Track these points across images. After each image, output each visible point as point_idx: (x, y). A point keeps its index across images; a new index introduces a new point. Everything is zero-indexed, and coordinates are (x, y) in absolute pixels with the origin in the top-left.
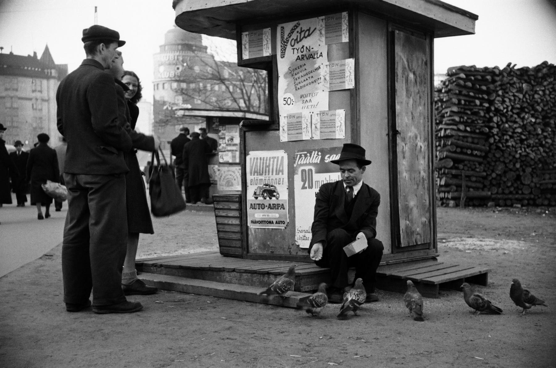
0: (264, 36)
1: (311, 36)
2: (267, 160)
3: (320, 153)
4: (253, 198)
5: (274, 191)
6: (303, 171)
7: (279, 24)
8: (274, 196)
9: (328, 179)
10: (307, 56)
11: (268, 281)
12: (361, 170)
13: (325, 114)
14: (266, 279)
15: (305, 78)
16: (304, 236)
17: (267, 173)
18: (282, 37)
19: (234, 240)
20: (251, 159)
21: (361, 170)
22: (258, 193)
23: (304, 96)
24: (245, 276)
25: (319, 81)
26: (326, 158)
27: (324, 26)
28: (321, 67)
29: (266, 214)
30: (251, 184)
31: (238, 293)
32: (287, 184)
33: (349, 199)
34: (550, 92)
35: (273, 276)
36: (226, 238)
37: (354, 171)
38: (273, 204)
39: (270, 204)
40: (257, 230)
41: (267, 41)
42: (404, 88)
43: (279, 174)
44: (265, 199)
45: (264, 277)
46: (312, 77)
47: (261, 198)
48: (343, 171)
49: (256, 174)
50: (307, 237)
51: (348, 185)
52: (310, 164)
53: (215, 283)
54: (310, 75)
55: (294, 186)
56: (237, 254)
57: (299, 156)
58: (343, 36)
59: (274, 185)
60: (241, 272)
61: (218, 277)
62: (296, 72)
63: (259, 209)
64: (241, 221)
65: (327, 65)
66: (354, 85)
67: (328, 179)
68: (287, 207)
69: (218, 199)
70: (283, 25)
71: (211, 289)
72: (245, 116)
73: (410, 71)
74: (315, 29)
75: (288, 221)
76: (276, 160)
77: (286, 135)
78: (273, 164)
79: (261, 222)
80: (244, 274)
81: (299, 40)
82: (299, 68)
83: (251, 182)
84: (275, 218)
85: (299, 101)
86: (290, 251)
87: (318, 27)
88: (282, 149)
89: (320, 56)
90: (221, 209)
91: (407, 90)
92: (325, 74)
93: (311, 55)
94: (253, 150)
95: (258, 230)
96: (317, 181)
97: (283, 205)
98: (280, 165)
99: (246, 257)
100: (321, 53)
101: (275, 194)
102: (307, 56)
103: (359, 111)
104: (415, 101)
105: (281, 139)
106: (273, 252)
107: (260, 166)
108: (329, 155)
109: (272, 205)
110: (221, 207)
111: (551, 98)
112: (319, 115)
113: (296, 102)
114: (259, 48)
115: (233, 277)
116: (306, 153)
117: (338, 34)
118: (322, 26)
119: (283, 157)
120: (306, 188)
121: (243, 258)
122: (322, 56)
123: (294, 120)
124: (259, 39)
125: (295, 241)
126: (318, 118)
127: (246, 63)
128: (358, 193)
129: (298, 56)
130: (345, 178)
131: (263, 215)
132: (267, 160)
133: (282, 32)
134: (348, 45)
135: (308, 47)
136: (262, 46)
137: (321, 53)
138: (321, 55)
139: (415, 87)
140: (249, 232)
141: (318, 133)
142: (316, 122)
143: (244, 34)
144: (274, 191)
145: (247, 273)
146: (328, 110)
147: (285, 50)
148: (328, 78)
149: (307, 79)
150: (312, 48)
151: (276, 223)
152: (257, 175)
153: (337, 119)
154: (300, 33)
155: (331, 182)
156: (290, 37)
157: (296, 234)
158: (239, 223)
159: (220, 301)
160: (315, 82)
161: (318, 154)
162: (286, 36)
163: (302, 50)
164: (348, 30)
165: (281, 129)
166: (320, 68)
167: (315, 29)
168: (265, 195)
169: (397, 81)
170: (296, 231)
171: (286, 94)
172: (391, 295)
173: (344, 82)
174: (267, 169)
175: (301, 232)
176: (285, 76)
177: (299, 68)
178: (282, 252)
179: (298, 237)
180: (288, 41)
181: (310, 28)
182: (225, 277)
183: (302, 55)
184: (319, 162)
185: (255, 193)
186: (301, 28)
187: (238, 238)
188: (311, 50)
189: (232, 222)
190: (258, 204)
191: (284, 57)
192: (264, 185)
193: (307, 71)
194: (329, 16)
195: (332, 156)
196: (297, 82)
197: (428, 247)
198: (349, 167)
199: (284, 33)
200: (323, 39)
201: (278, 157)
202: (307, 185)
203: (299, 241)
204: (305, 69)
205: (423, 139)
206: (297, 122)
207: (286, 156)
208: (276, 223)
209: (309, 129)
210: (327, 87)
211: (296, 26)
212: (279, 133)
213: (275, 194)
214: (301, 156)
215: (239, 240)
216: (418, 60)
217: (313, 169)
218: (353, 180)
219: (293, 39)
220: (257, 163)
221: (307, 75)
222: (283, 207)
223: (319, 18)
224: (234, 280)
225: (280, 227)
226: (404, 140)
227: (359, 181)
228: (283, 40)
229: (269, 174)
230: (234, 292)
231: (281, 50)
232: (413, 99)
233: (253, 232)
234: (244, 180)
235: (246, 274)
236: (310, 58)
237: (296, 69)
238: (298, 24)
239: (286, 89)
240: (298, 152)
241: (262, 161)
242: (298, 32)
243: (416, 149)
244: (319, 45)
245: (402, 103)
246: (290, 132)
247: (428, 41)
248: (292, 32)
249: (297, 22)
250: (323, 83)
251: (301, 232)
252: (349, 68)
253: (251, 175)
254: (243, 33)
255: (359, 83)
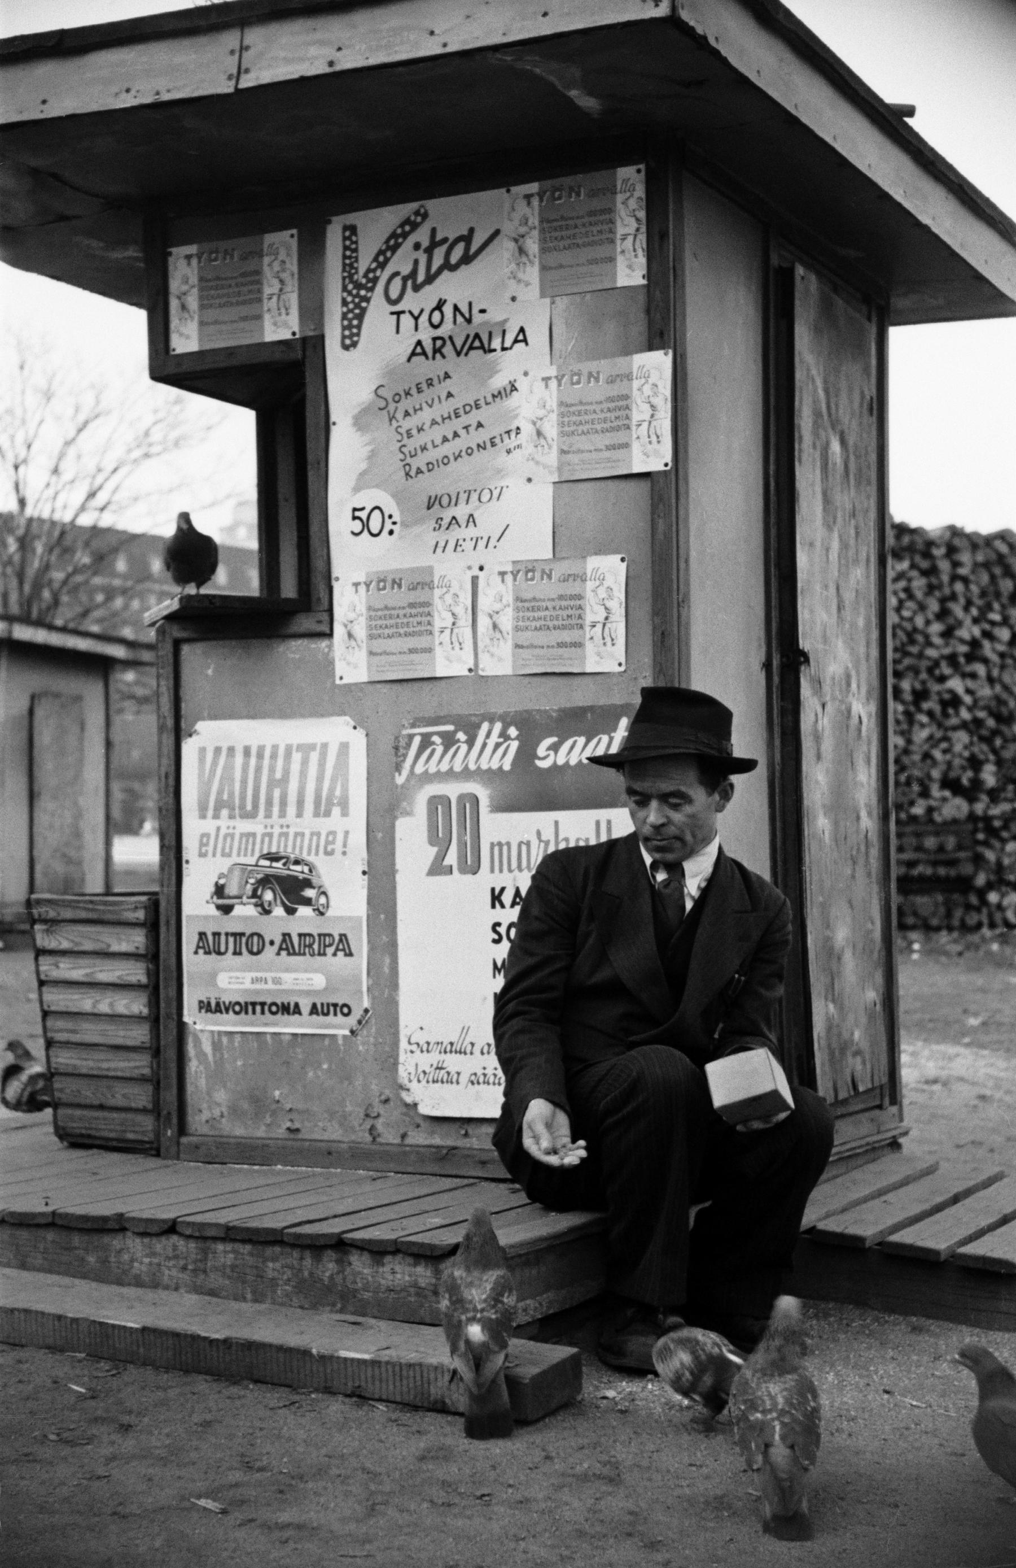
0: (266, 260)
1: (476, 265)
2: (274, 756)
3: (513, 732)
4: (212, 910)
5: (308, 883)
6: (436, 803)
7: (337, 214)
8: (308, 902)
9: (548, 834)
10: (459, 344)
11: (339, 1279)
12: (717, 797)
13: (538, 575)
14: (329, 1266)
15: (447, 429)
16: (439, 1068)
17: (276, 810)
18: (349, 267)
19: (117, 1078)
20: (203, 751)
21: (717, 797)
22: (232, 889)
23: (445, 501)
24: (224, 1254)
25: (511, 442)
26: (541, 751)
27: (534, 220)
28: (522, 384)
29: (269, 975)
30: (202, 855)
31: (212, 1342)
32: (364, 854)
33: (671, 913)
34: (901, 602)
35: (366, 1257)
36: (84, 1071)
37: (687, 799)
38: (300, 935)
39: (286, 936)
40: (225, 1040)
41: (282, 282)
42: (818, 489)
43: (328, 814)
44: (267, 912)
45: (317, 1258)
46: (480, 425)
47: (246, 911)
48: (642, 800)
49: (225, 812)
50: (453, 1071)
51: (658, 856)
52: (467, 774)
53: (83, 1286)
54: (473, 418)
55: (393, 864)
56: (130, 1136)
57: (417, 741)
58: (621, 262)
59: (305, 856)
60: (205, 1239)
61: (91, 1259)
62: (406, 404)
63: (237, 953)
64: (154, 1002)
65: (546, 380)
66: (668, 457)
67: (548, 834)
68: (361, 945)
69: (52, 914)
70: (351, 218)
71: (75, 1321)
72: (10, 632)
73: (833, 428)
74: (497, 233)
75: (366, 1003)
76: (314, 757)
77: (361, 656)
78: (303, 774)
79: (245, 1008)
80: (220, 1247)
81: (421, 277)
82: (419, 391)
83: (202, 845)
84: (308, 993)
85: (419, 521)
86: (372, 1129)
87: (509, 228)
88: (342, 713)
89: (516, 341)
90: (64, 953)
91: (827, 500)
92: (541, 413)
93: (477, 336)
94: (214, 717)
95: (231, 1042)
96: (500, 844)
97: (343, 937)
98: (334, 780)
99: (173, 1150)
100: (522, 330)
101: (309, 893)
102: (459, 344)
103: (687, 561)
104: (844, 546)
105: (338, 675)
106: (297, 1130)
107: (244, 782)
108: (555, 739)
109: (210, 938)
110: (65, 945)
111: (902, 618)
112: (509, 578)
113: (405, 525)
114: (245, 310)
115: (168, 1258)
116: (450, 728)
117: (601, 252)
118: (525, 221)
119: (344, 748)
120: (450, 870)
121: (158, 1155)
122: (525, 341)
123: (398, 598)
124: (244, 275)
125: (401, 1087)
126: (507, 591)
127: (186, 367)
128: (705, 892)
129: (419, 343)
130: (647, 830)
131: (253, 981)
132: (274, 756)
133: (346, 248)
134: (642, 298)
135: (465, 309)
136: (260, 300)
137: (522, 330)
138: (522, 337)
139: (846, 492)
140: (191, 1050)
141: (506, 648)
142: (497, 606)
143: (180, 252)
144: (308, 883)
145: (234, 1240)
146: (551, 556)
147: (360, 317)
148: (551, 429)
149: (456, 435)
150: (483, 311)
151: (314, 1010)
152: (231, 817)
153: (589, 594)
154: (429, 251)
155: (562, 846)
156: (382, 266)
157: (402, 1058)
158: (145, 1011)
159: (126, 1377)
160: (493, 445)
161: (504, 735)
162: (364, 263)
163: (436, 317)
164: (642, 237)
165: (339, 630)
166: (514, 388)
167: (497, 233)
168: (268, 896)
169: (800, 461)
170: (403, 1044)
171: (362, 494)
172: (826, 1315)
173: (626, 446)
174: (277, 793)
175: (426, 1048)
176: (360, 422)
177: (419, 391)
178: (333, 1132)
179: (412, 1070)
180: (375, 280)
181: (472, 230)
182: (126, 1257)
183: (434, 339)
184: (507, 767)
185: (219, 891)
186: (434, 231)
187: (136, 1073)
188: (477, 318)
189: (111, 1005)
190: (234, 935)
191: (354, 344)
192: (264, 857)
193: (456, 403)
194: (557, 182)
195: (569, 743)
196: (412, 444)
197: (878, 1103)
198: (666, 787)
199: (356, 250)
200: (533, 273)
201: (325, 746)
202: (452, 858)
203: (414, 1086)
204: (450, 395)
205: (864, 690)
206: (412, 605)
207: (358, 741)
208: (314, 1010)
209: (465, 632)
210: (545, 467)
211: (411, 225)
212: (330, 647)
213: (309, 893)
214: (426, 742)
215: (143, 1079)
216: (851, 390)
217: (483, 794)
218: (679, 838)
219: (396, 274)
220: (229, 768)
221: (457, 416)
222: (344, 945)
223: (514, 189)
224: (170, 1273)
225: (327, 1027)
226: (818, 683)
227: (707, 841)
228: (351, 276)
229: (283, 814)
230: (195, 1338)
231: (344, 316)
232: (840, 536)
233: (207, 1048)
234: (171, 840)
235: (229, 1247)
236: (471, 348)
237: (408, 394)
238: (417, 213)
239: (363, 474)
240: (413, 726)
241: (253, 761)
242: (417, 246)
243: (847, 726)
244: (514, 299)
245: (811, 545)
246: (379, 645)
247: (873, 330)
248: (392, 245)
249: (414, 206)
250: (529, 449)
251: (426, 1048)
252: (647, 390)
253: (203, 816)
254: (174, 250)
255: (686, 451)
